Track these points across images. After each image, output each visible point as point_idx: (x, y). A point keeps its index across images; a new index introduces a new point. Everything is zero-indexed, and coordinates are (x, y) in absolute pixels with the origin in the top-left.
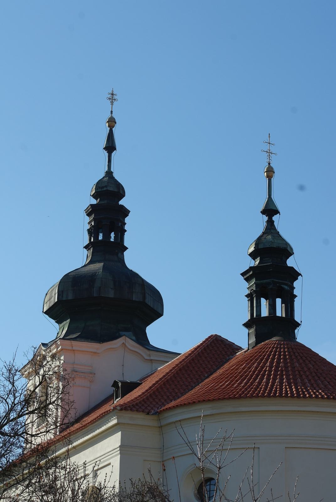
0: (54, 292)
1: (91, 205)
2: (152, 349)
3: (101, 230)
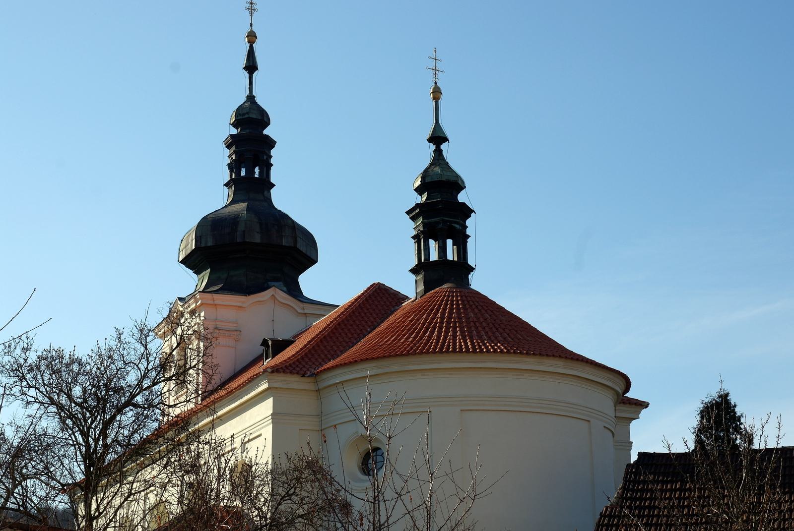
0: (190, 238)
1: (231, 135)
3: (243, 165)
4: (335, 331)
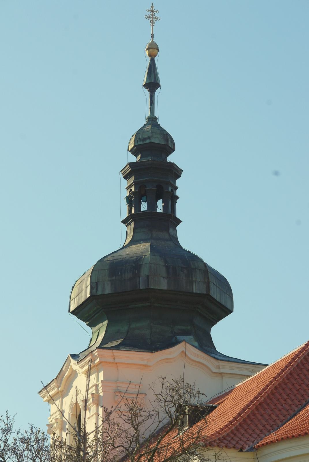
0: (84, 285)
1: (130, 164)
2: (222, 358)
3: (144, 198)
4: (272, 396)
